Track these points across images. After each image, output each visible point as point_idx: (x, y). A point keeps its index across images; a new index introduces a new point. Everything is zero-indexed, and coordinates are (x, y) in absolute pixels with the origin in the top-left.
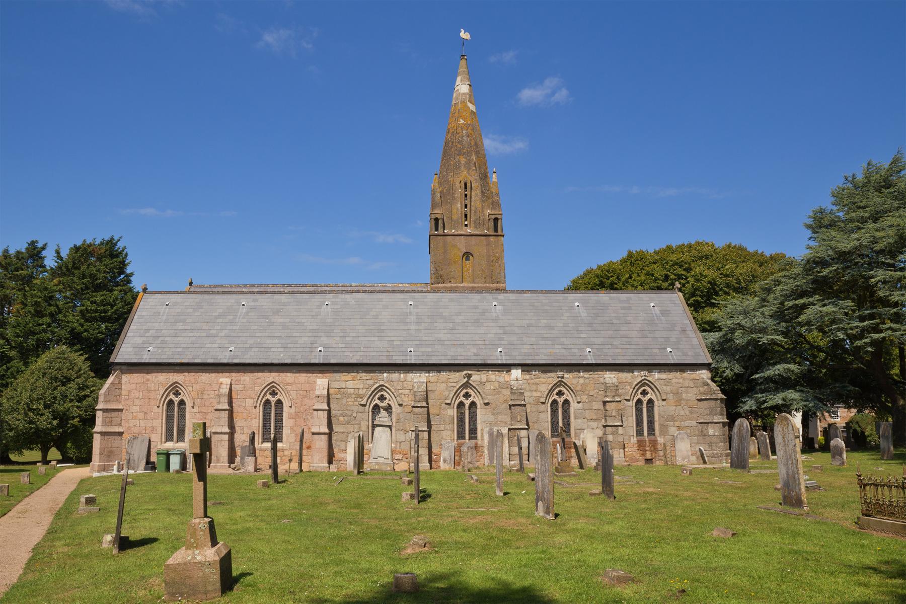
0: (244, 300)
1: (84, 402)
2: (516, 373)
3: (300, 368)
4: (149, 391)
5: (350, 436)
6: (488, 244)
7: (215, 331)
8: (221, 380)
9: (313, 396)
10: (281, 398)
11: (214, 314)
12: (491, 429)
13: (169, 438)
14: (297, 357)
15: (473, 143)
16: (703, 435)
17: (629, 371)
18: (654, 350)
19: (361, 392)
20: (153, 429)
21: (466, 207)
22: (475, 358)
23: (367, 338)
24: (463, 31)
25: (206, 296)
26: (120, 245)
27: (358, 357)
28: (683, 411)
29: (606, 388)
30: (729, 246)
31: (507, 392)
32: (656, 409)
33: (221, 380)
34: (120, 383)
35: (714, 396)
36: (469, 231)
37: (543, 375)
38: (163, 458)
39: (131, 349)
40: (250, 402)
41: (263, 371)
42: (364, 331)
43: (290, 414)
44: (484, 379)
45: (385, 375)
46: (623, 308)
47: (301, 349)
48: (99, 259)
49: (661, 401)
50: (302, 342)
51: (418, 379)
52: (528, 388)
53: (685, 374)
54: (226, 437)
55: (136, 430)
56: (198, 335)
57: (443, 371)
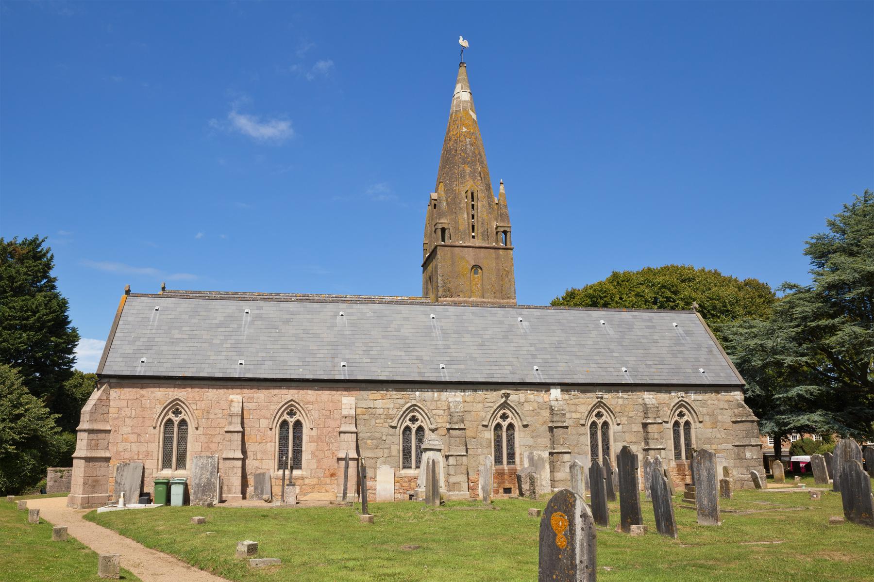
0: (247, 306)
1: (19, 422)
2: (556, 393)
3: (323, 385)
4: (144, 409)
5: (379, 461)
6: (497, 258)
7: (218, 341)
8: (231, 397)
9: (337, 416)
10: (301, 419)
11: (214, 322)
12: (531, 453)
13: (166, 463)
14: (319, 372)
15: (477, 152)
16: (740, 458)
17: (666, 392)
18: (688, 371)
19: (391, 412)
20: (148, 454)
21: (473, 218)
22: (512, 376)
23: (392, 353)
24: (461, 39)
25: (201, 302)
26: (44, 246)
27: (387, 374)
28: (721, 434)
29: (646, 410)
30: (703, 270)
31: (546, 413)
32: (693, 431)
33: (231, 397)
34: (108, 399)
35: (750, 418)
36: (478, 242)
37: (582, 395)
38: (162, 488)
39: (120, 359)
40: (264, 423)
41: (280, 388)
42: (388, 345)
43: (311, 437)
44: (523, 400)
45: (417, 393)
46: (648, 327)
47: (322, 364)
48: (21, 261)
49: (698, 423)
50: (322, 356)
51: (454, 397)
52: (567, 409)
53: (719, 396)
54: (240, 463)
55: (127, 455)
56: (199, 345)
57: (480, 390)
